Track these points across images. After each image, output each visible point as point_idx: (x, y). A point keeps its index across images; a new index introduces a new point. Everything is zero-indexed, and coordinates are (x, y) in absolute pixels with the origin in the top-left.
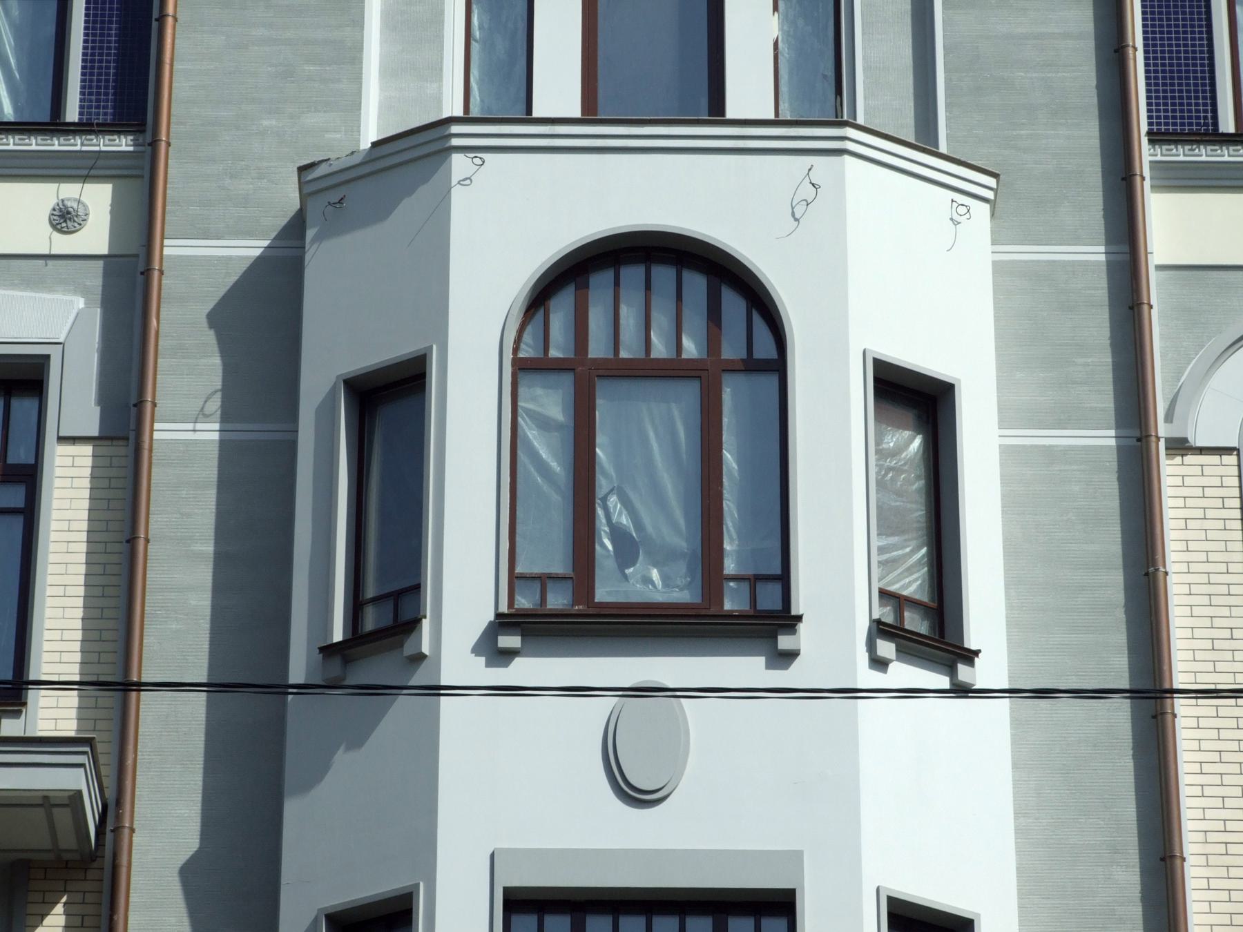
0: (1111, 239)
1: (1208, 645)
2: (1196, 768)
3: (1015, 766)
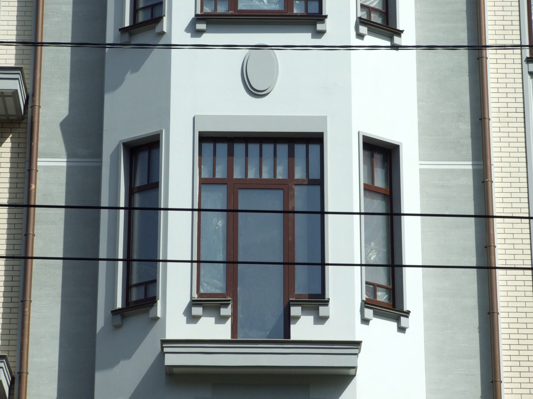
1: (518, 386)
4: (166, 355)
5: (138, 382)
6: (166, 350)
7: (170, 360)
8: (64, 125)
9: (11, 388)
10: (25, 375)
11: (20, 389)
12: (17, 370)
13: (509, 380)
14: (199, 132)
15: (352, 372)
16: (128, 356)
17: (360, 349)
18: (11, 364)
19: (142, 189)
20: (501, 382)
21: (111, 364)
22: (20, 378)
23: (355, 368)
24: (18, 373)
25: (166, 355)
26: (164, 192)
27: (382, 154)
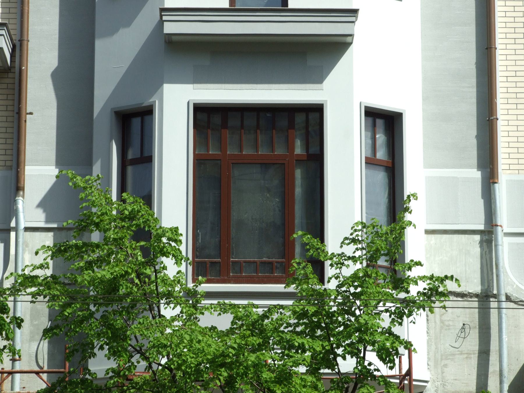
0: (481, 166)
1: (513, 52)
2: (506, 145)
3: (424, 120)
4: (165, 23)
5: (137, 49)
6: (164, 18)
7: (169, 28)
8: (55, 75)
9: (12, 55)
10: (25, 42)
11: (21, 56)
12: (18, 38)
13: (504, 46)
14: (194, 104)
15: (349, 39)
16: (128, 23)
17: (357, 17)
18: (12, 32)
19: (135, 162)
20: (496, 49)
21: (112, 31)
22: (21, 45)
23: (351, 35)
24: (19, 41)
25: (165, 23)
26: (158, 135)
27: (386, 123)
